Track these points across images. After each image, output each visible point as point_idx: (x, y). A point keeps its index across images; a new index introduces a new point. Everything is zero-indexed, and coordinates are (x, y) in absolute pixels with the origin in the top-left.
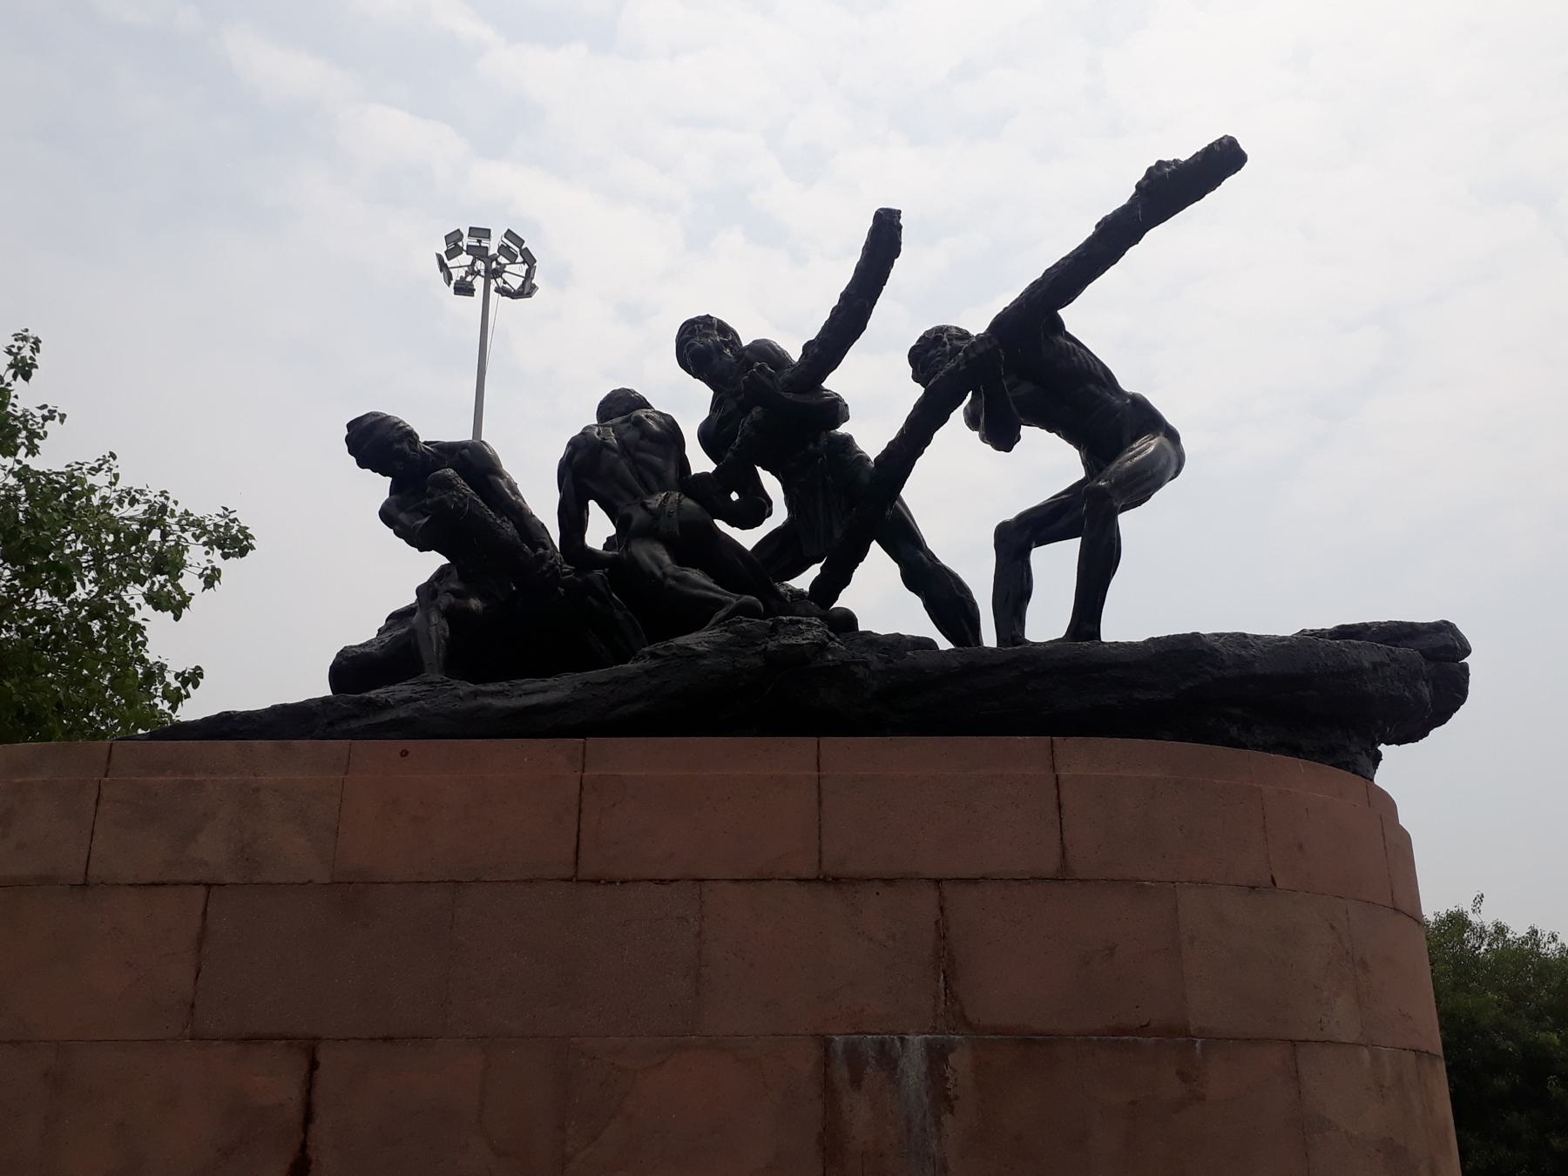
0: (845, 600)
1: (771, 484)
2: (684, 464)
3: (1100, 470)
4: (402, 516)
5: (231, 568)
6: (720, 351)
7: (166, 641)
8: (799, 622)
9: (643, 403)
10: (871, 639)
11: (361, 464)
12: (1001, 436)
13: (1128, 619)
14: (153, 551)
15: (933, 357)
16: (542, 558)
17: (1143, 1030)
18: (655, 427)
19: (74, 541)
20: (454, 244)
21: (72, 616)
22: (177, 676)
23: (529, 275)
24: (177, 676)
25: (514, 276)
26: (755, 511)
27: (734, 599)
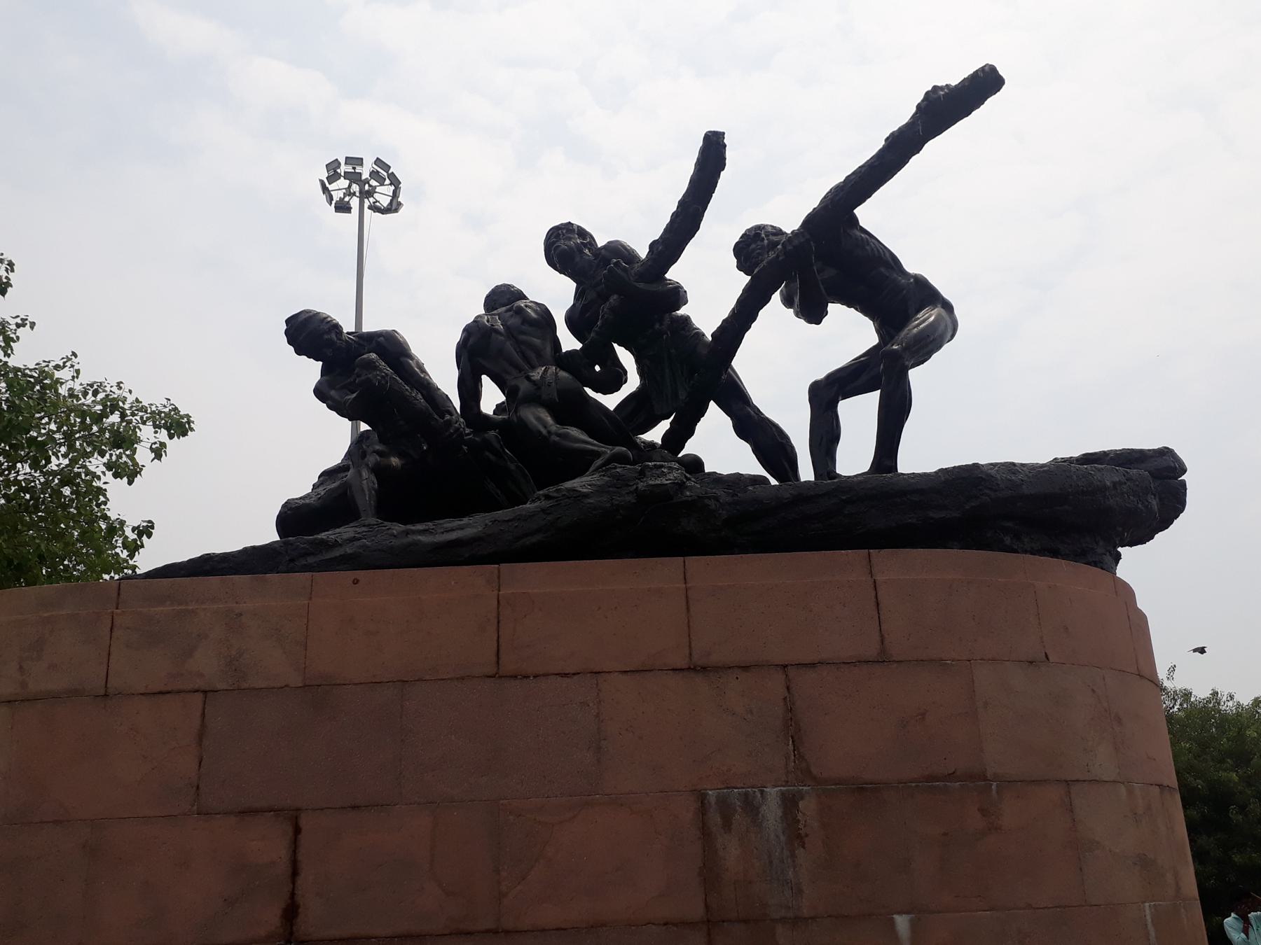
0: (690, 448)
1: (625, 357)
2: (556, 343)
3: (892, 337)
4: (333, 393)
5: (174, 445)
6: (581, 252)
7: (123, 502)
8: (662, 466)
9: (521, 296)
10: (716, 478)
11: (299, 352)
12: (813, 313)
13: (920, 454)
14: (113, 430)
15: (754, 250)
16: (449, 423)
17: (951, 776)
18: (533, 314)
19: (48, 423)
20: (333, 171)
21: (46, 484)
22: (134, 530)
23: (395, 195)
24: (134, 530)
25: (383, 195)
26: (614, 379)
27: (608, 450)
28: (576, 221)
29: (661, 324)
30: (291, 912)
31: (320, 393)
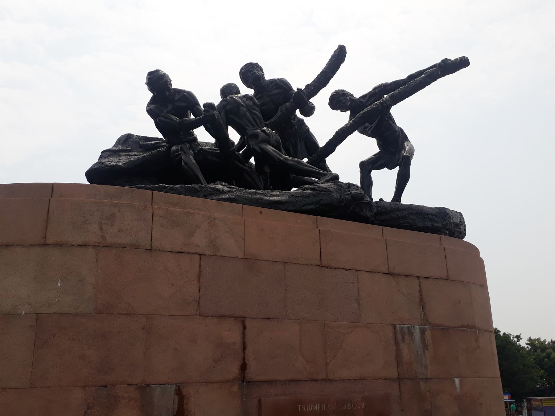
13: (405, 200)
15: (342, 100)
17: (468, 326)
28: (260, 64)
30: (244, 367)
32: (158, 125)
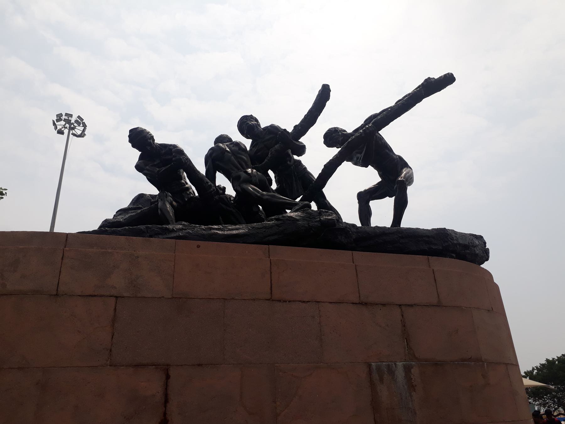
13: (405, 223)
15: (334, 136)
17: (470, 359)
23: (84, 131)
28: (254, 115)
29: (290, 162)
31: (139, 168)
32: (152, 180)
